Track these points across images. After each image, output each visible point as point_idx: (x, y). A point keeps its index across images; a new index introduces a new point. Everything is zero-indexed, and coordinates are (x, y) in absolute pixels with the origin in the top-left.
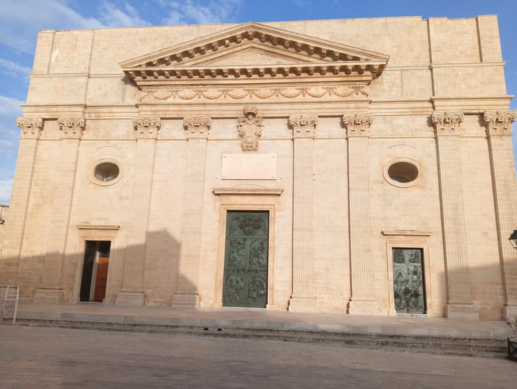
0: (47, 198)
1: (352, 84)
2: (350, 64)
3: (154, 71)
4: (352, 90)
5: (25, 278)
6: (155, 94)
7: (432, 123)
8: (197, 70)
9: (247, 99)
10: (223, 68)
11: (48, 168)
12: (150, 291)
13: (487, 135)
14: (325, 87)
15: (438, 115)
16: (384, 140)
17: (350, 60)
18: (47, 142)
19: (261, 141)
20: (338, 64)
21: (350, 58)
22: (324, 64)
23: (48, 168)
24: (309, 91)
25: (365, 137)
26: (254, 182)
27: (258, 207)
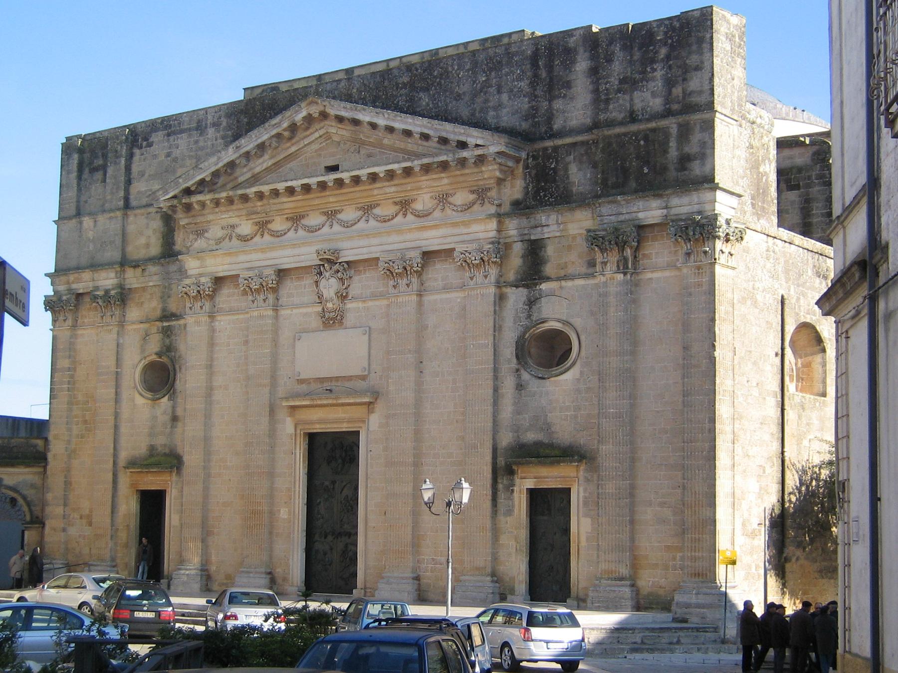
27: (345, 425)
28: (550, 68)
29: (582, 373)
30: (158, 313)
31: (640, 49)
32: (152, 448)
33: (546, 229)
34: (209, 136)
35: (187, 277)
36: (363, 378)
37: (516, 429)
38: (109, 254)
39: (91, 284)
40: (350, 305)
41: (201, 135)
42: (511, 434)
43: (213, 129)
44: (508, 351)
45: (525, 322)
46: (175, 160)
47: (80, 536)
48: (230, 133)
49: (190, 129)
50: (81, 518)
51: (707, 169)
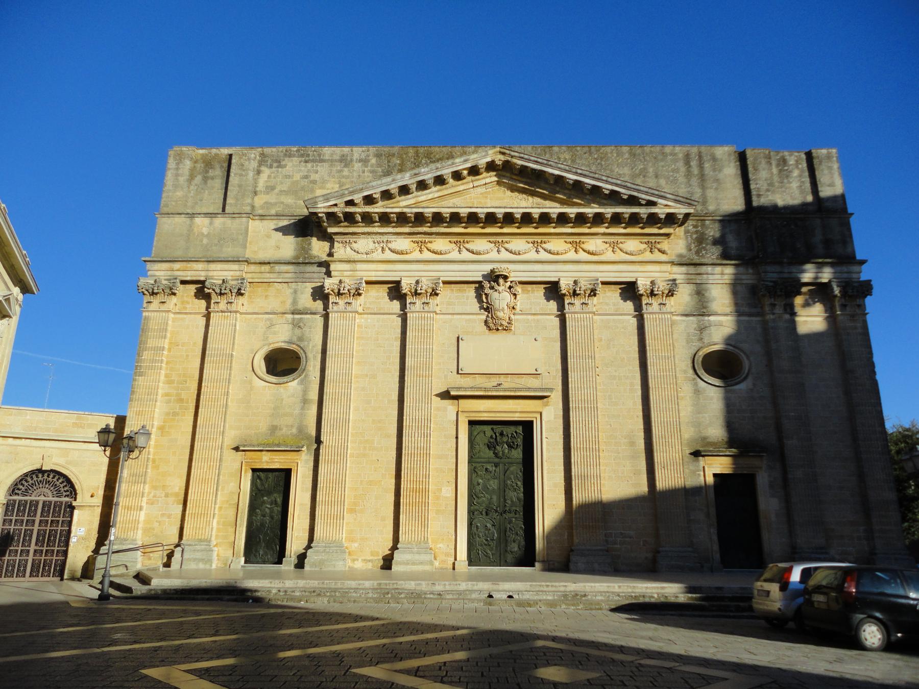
0: (187, 402)
1: (646, 239)
2: (643, 211)
3: (355, 213)
4: (645, 246)
5: (153, 529)
6: (354, 246)
7: (320, 294)
8: (422, 213)
9: (494, 255)
10: (442, 210)
11: (187, 356)
12: (356, 545)
13: (401, 310)
14: (568, 240)
15: (330, 284)
16: (540, 317)
17: (642, 205)
18: (185, 316)
19: (517, 317)
20: (626, 211)
21: (643, 202)
22: (590, 210)
23: (187, 356)
24: (585, 246)
25: (667, 313)
26: (515, 378)
27: (517, 415)
28: (701, 166)
29: (754, 385)
30: (288, 306)
31: (778, 165)
32: (274, 429)
33: (711, 277)
34: (355, 168)
35: (146, 276)
36: (536, 375)
37: (697, 425)
38: (229, 249)
39: (203, 273)
40: (99, 557)
41: (346, 166)
42: (692, 429)
43: (360, 164)
44: (460, 182)
45: (699, 344)
46: (314, 182)
47: (163, 515)
48: (380, 170)
49: (332, 161)
50: (167, 496)
51: (849, 250)
